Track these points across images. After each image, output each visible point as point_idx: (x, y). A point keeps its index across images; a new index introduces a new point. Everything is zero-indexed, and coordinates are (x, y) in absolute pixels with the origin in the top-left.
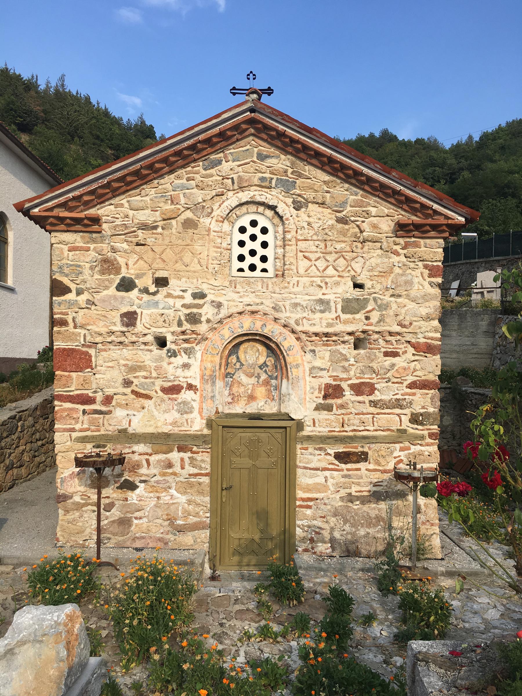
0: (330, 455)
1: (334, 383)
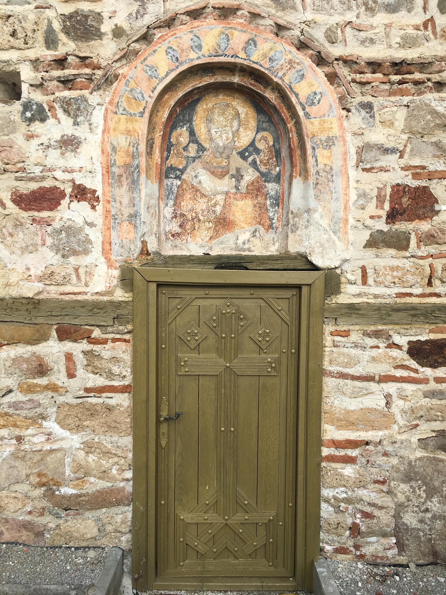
0: (399, 347)
1: (414, 183)
